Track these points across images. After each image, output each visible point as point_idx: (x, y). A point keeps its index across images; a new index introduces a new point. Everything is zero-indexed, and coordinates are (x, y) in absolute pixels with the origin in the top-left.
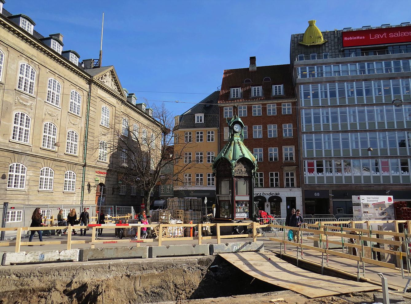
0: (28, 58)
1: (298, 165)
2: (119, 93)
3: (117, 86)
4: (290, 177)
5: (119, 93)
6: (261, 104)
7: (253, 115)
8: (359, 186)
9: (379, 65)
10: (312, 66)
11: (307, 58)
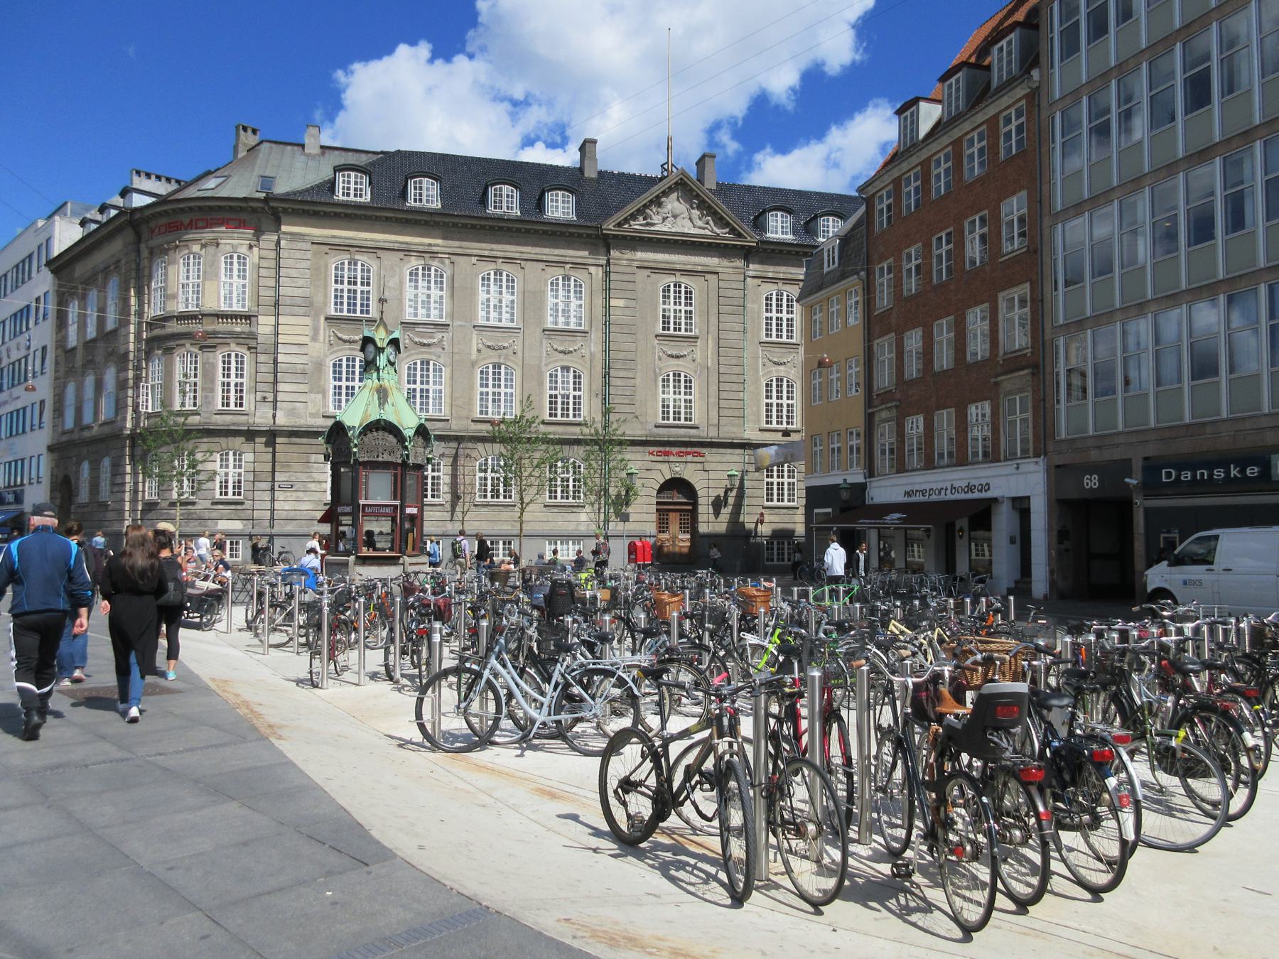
0: (421, 253)
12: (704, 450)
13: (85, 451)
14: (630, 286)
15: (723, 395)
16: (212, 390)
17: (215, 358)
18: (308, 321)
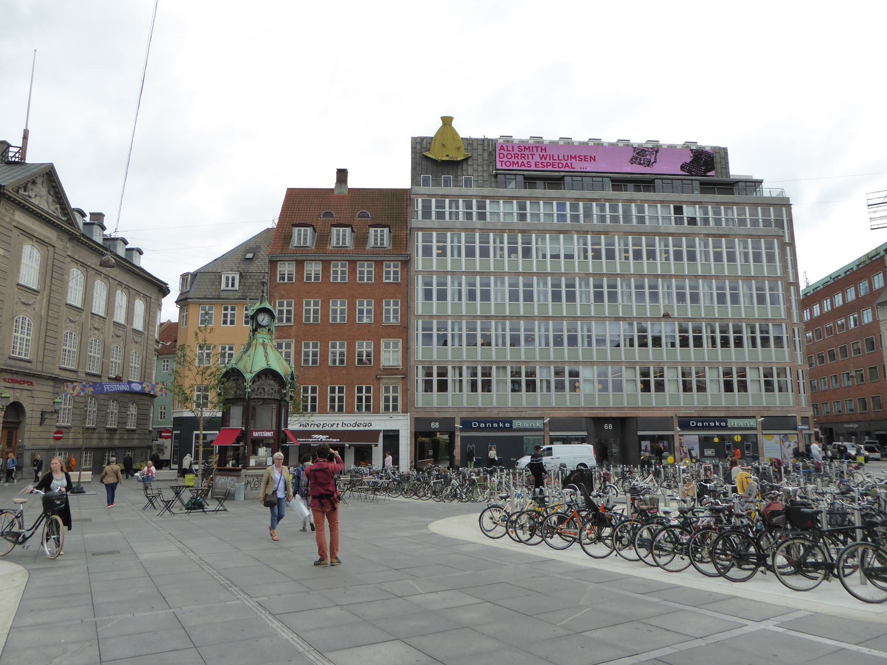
1: (403, 373)
2: (63, 218)
3: (60, 203)
4: (391, 395)
5: (63, 218)
6: (399, 261)
7: (331, 281)
8: (503, 410)
9: (508, 206)
10: (442, 197)
11: (437, 184)
12: (34, 381)
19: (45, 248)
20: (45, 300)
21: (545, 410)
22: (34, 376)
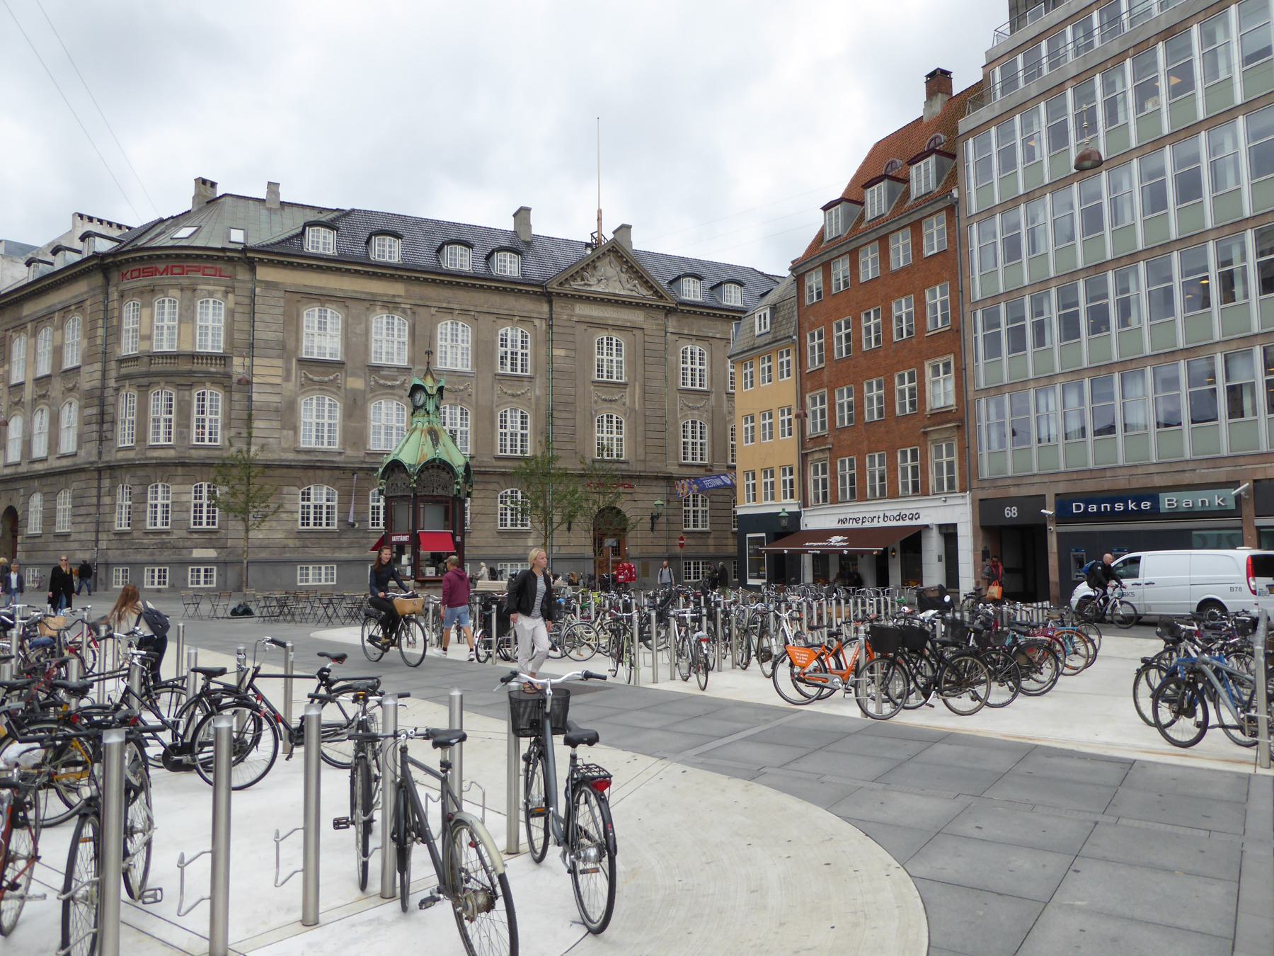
8: (1140, 471)
12: (634, 483)
13: (36, 483)
14: (570, 338)
15: (649, 435)
16: (188, 427)
17: (191, 396)
18: (279, 362)
19: (630, 334)
20: (637, 391)
21: (1242, 461)
22: (631, 477)
